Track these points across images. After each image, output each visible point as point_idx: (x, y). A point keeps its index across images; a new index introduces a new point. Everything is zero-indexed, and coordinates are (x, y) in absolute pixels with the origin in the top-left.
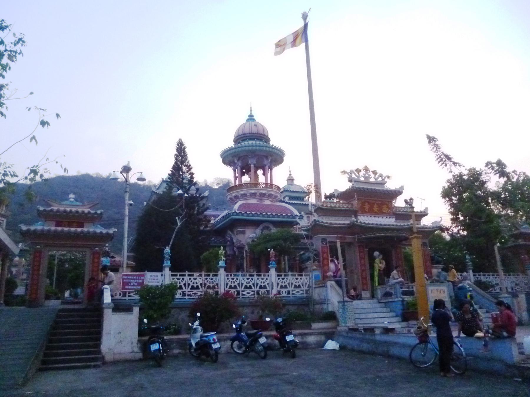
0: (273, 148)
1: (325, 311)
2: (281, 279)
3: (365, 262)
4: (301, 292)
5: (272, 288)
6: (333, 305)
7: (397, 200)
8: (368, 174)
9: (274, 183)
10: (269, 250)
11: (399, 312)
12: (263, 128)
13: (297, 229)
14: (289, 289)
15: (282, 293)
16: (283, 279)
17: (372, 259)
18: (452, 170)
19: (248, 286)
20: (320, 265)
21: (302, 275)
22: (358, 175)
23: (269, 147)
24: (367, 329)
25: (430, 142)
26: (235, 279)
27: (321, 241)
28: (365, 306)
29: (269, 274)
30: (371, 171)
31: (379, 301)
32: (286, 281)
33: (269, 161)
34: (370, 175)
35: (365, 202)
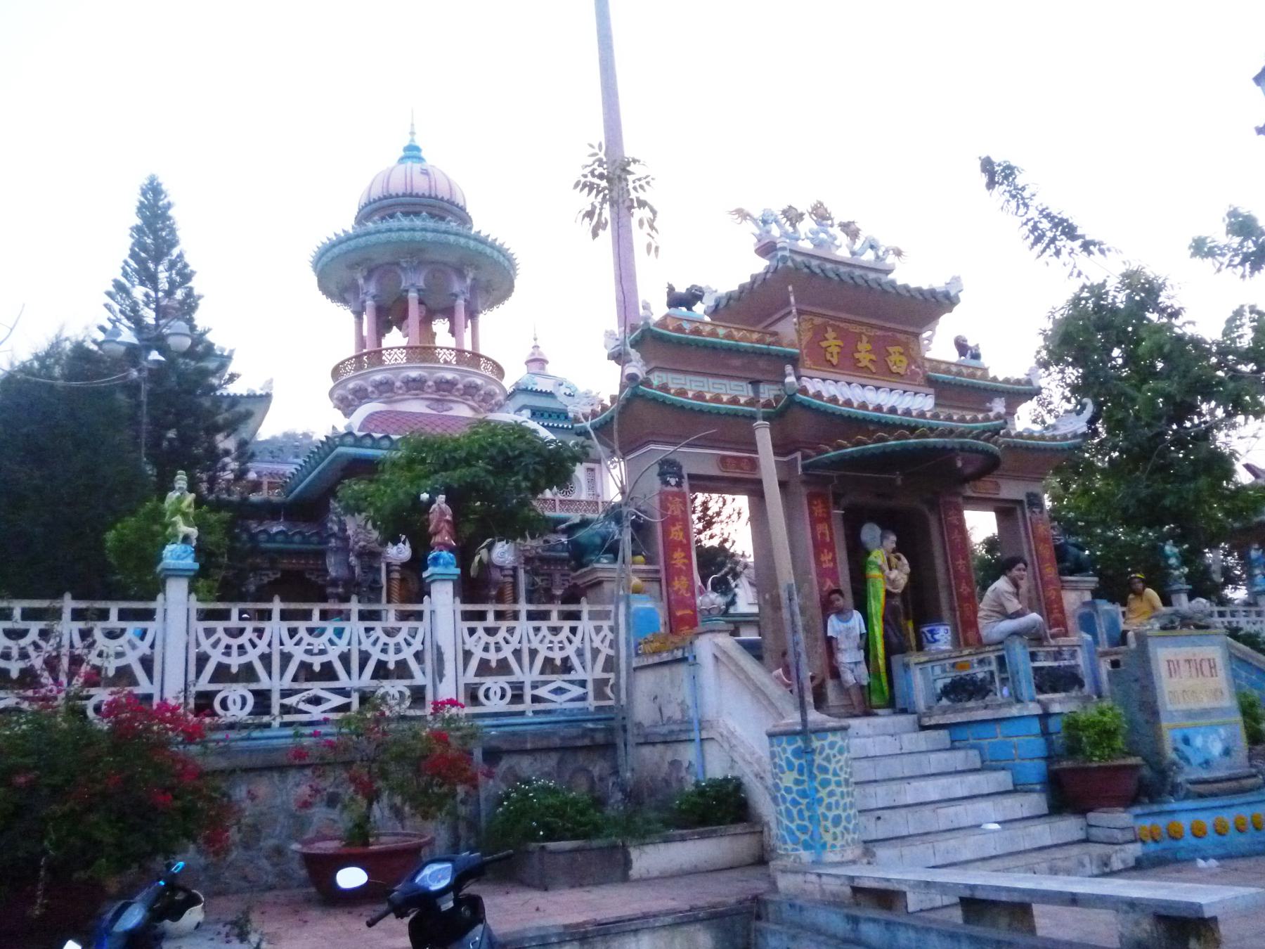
0: (479, 240)
1: (691, 779)
2: (220, 633)
3: (834, 560)
4: (576, 691)
5: (439, 673)
6: (732, 747)
7: (938, 328)
8: (826, 232)
9: (482, 351)
10: (425, 496)
11: (1035, 769)
12: (450, 186)
13: (557, 503)
14: (518, 676)
15: (487, 697)
16: (491, 631)
17: (858, 555)
18: (1079, 267)
19: (317, 668)
20: (657, 571)
21: (576, 616)
22: (791, 230)
23: (468, 237)
24: (994, 903)
25: (991, 184)
26: (502, 633)
27: (656, 469)
28: (874, 746)
29: (425, 606)
30: (836, 222)
31: (919, 720)
32: (398, 644)
33: (469, 281)
34: (835, 239)
35: (824, 328)
